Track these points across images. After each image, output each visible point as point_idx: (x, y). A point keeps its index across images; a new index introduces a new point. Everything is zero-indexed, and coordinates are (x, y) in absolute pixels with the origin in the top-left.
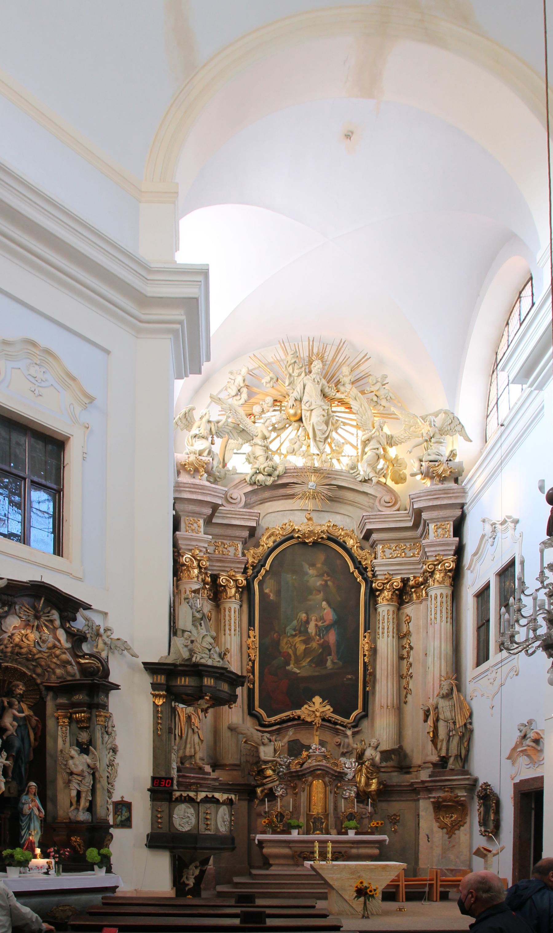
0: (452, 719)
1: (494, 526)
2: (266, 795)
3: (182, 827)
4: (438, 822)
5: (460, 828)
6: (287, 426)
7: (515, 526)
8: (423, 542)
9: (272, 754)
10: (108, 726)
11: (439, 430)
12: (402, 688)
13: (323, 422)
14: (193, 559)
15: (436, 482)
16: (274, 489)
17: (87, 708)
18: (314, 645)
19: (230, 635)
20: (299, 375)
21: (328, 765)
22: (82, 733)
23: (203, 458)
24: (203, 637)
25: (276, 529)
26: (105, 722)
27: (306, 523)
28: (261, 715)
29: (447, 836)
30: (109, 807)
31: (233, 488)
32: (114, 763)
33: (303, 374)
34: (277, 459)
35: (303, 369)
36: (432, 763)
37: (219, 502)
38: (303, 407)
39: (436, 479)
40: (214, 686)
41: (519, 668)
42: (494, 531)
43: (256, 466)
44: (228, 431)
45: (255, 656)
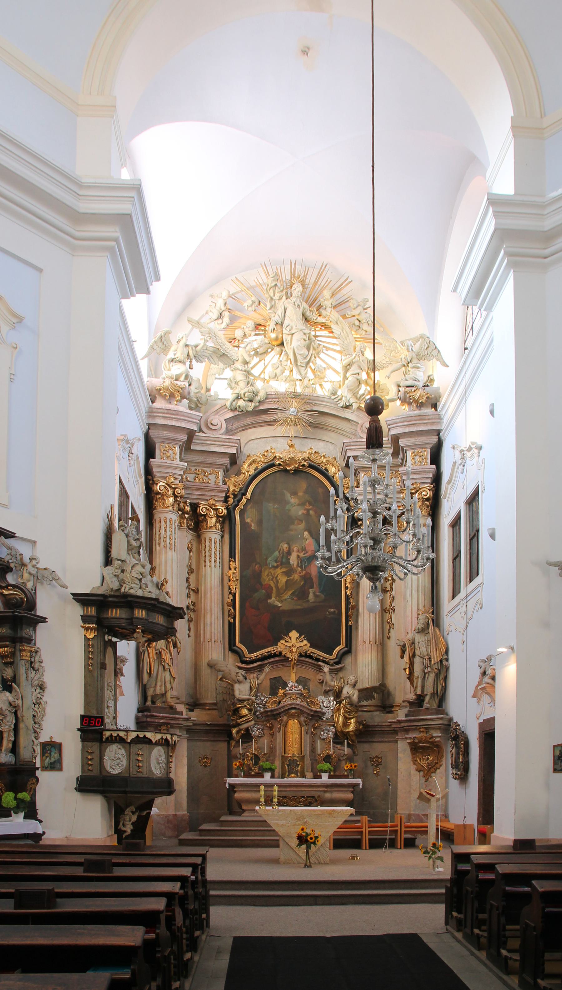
0: (428, 655)
1: (462, 453)
2: (243, 737)
3: (113, 769)
4: (416, 765)
5: (436, 770)
6: (269, 350)
7: (479, 453)
8: (401, 469)
9: (248, 693)
10: (34, 661)
11: (416, 355)
12: (385, 623)
13: (304, 346)
14: (168, 487)
15: (413, 408)
16: (257, 415)
17: (10, 642)
18: (296, 577)
19: (210, 566)
20: (280, 299)
21: (302, 704)
22: (7, 669)
23: (179, 383)
24: (133, 566)
25: (257, 456)
26: (31, 657)
27: (288, 450)
28: (242, 651)
29: (424, 779)
30: (34, 747)
31: (213, 414)
32: (41, 700)
33: (284, 298)
34: (259, 385)
35: (284, 292)
36: (409, 702)
37: (195, 428)
38: (284, 331)
39: (413, 405)
40: (146, 618)
41: (482, 600)
42: (463, 459)
43: (237, 391)
44: (208, 355)
45: (235, 588)
